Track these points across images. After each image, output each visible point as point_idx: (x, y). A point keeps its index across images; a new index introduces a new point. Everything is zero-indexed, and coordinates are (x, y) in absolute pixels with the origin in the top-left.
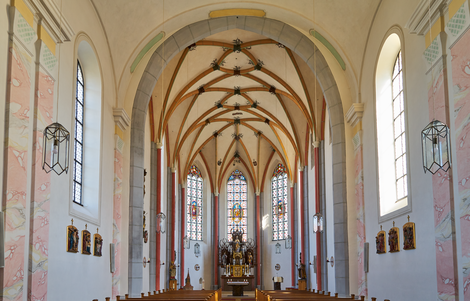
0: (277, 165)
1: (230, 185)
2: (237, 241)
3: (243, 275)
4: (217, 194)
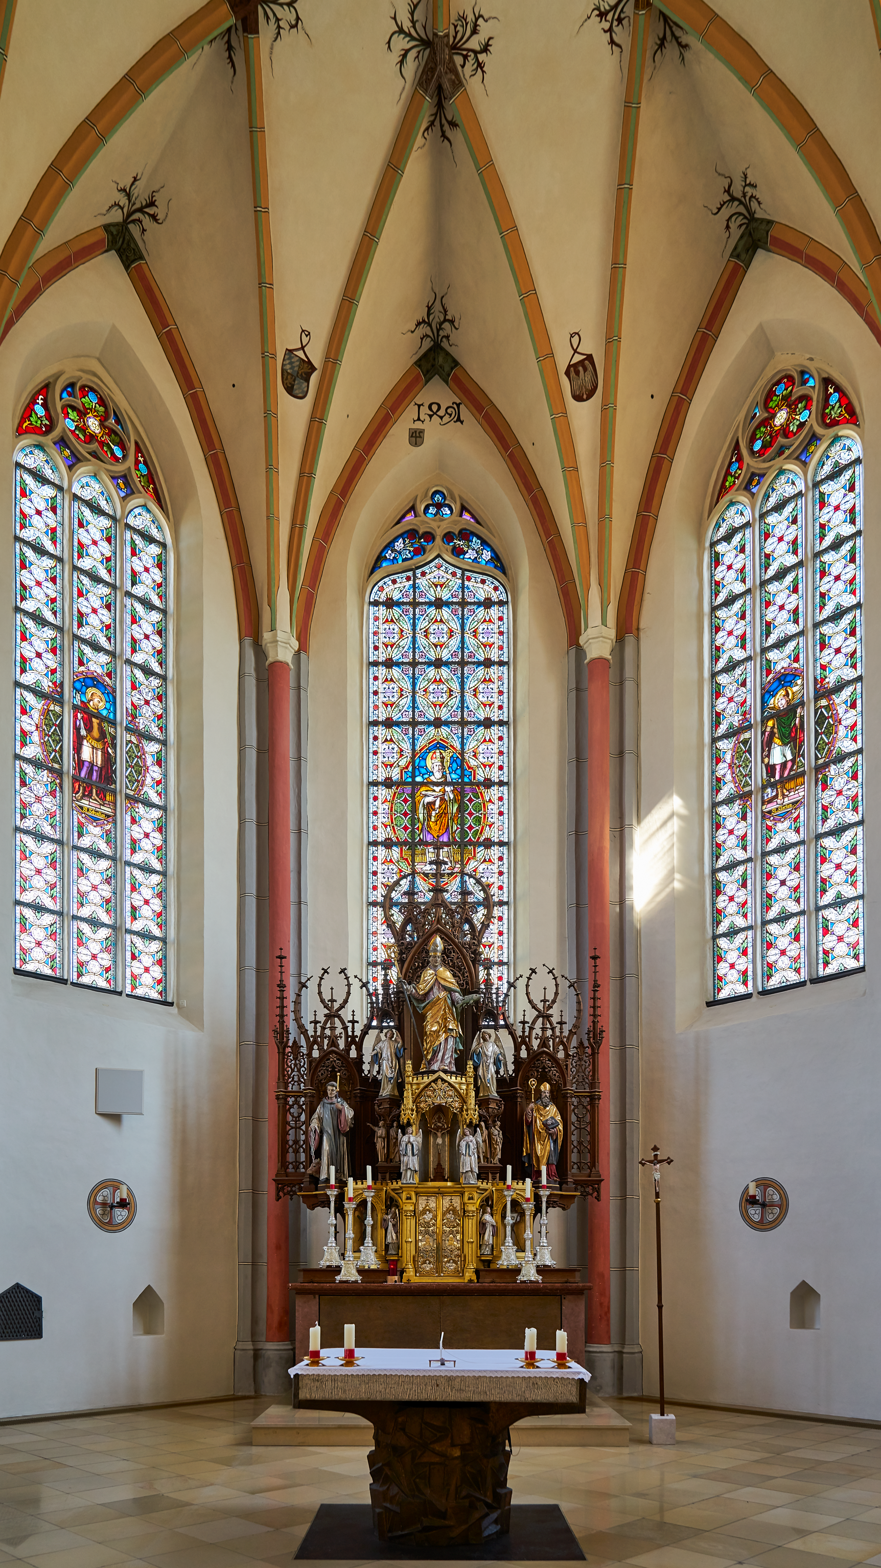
0: (762, 384)
1: (390, 603)
2: (439, 976)
3: (486, 1266)
4: (283, 646)
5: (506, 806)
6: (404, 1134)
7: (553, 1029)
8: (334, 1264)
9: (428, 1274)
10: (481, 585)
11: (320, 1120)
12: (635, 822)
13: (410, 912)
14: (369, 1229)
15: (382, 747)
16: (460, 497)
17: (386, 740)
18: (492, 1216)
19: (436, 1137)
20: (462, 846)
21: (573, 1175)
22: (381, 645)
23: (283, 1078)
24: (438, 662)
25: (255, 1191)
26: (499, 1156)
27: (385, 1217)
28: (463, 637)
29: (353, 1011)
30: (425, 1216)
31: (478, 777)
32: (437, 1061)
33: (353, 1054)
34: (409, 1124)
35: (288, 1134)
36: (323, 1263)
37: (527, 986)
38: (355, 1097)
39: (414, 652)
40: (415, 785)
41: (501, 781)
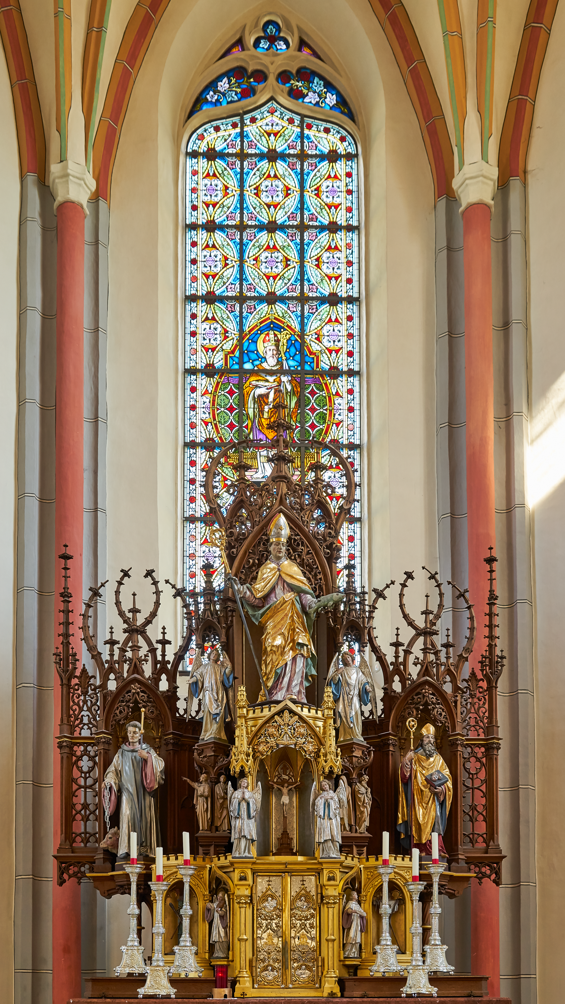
2: (281, 572)
4: (76, 182)
5: (357, 400)
6: (235, 788)
7: (436, 653)
8: (136, 970)
9: (271, 984)
10: (324, 135)
11: (118, 774)
12: (525, 409)
13: (242, 492)
14: (186, 923)
15: (202, 327)
16: (299, 28)
17: (207, 319)
18: (360, 904)
19: (280, 794)
20: (303, 449)
21: (465, 851)
22: (200, 205)
23: (69, 720)
24: (271, 226)
25: (36, 877)
26: (367, 823)
27: (209, 905)
28: (302, 196)
29: (164, 628)
30: (266, 904)
31: (322, 364)
32: (281, 689)
33: (164, 685)
34: (243, 774)
35: (74, 794)
36: (121, 970)
37: (401, 595)
38: (167, 744)
39: (242, 214)
40: (243, 374)
41: (350, 370)
